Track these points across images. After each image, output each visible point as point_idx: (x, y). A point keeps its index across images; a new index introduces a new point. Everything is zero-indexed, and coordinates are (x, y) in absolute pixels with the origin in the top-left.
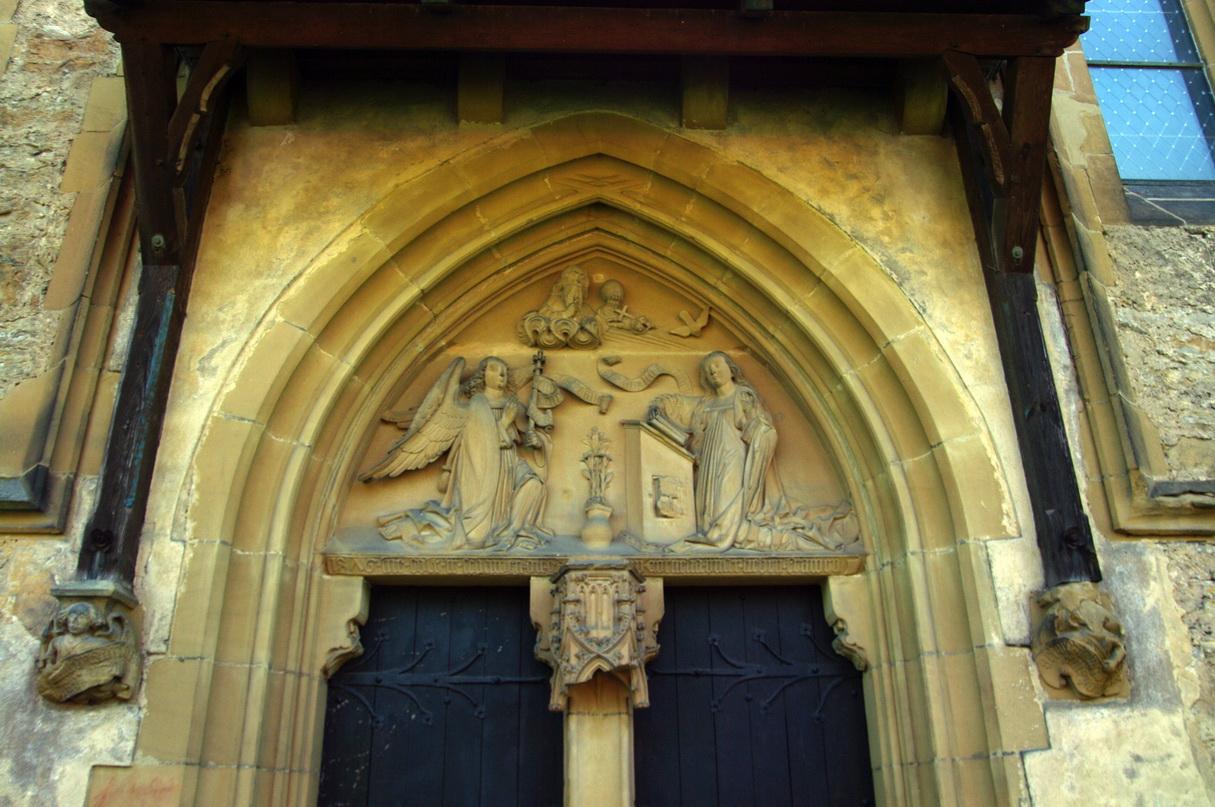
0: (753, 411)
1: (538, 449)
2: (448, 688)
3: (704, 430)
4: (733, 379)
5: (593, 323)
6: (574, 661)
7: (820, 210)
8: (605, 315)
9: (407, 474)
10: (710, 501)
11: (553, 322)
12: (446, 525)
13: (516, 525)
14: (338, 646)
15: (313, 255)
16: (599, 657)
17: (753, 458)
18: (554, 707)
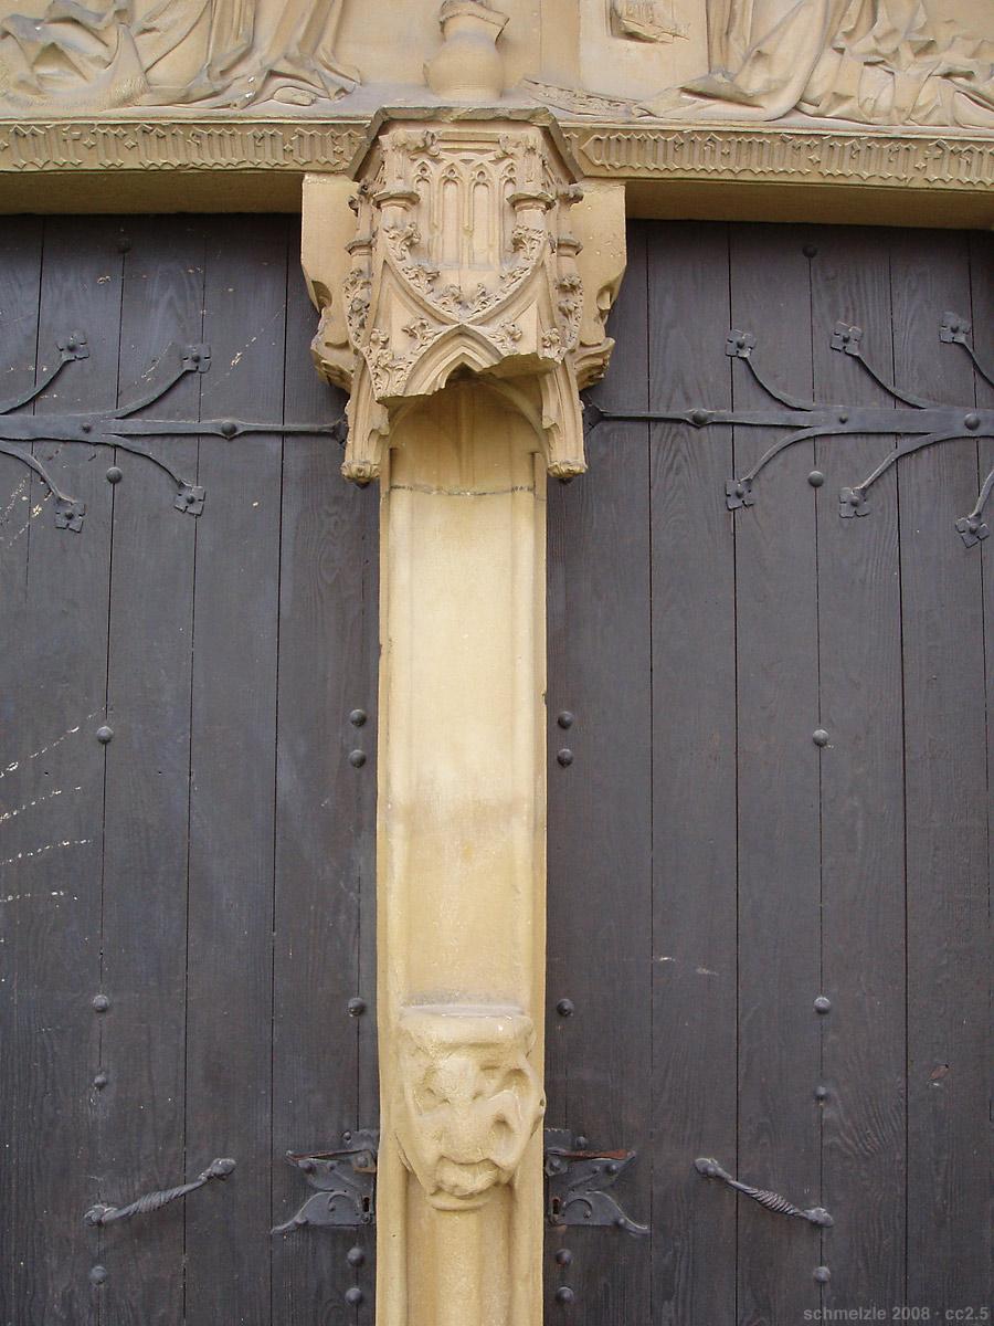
2: (116, 447)
6: (399, 342)
12: (97, 49)
13: (267, 51)
16: (462, 332)
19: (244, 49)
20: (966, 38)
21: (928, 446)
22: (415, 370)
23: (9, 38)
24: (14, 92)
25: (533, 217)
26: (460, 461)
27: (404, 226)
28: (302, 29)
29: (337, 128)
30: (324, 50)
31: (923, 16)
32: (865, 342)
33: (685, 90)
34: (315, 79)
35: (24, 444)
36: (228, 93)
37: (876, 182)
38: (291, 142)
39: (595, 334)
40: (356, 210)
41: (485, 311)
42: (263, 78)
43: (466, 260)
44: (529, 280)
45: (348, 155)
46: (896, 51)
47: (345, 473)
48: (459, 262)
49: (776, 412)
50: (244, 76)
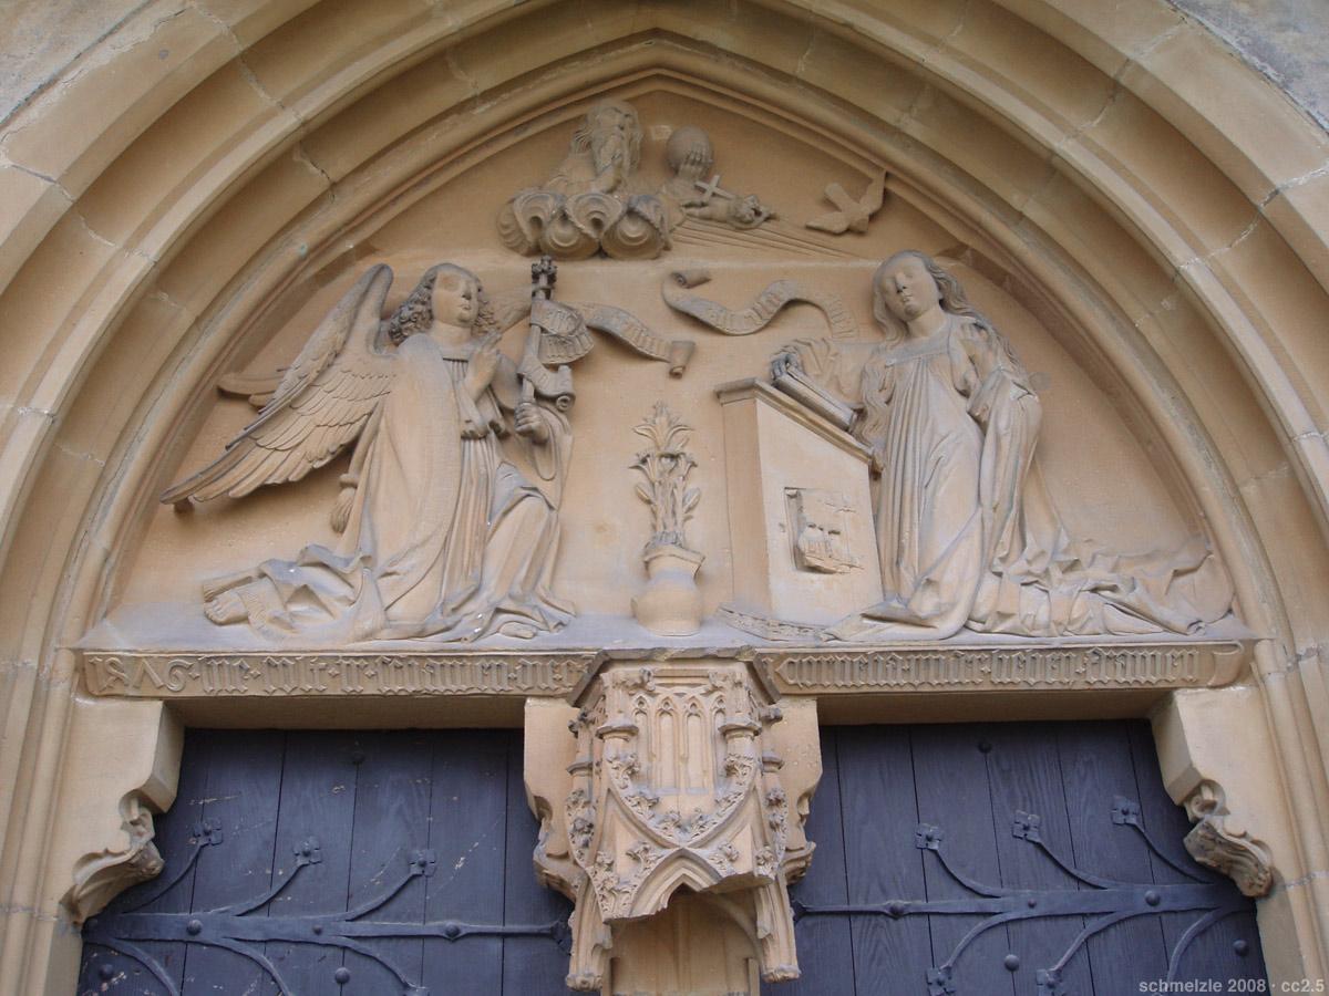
0: (990, 356)
1: (538, 441)
2: (345, 948)
3: (888, 402)
4: (942, 303)
5: (653, 203)
6: (623, 865)
9: (267, 493)
10: (912, 536)
11: (571, 201)
12: (344, 590)
13: (492, 592)
14: (100, 850)
17: (998, 446)
18: (579, 980)
19: (473, 589)
20: (1106, 555)
21: (1114, 924)
22: (640, 893)
23: (266, 578)
25: (744, 746)
26: (677, 965)
27: (626, 757)
29: (559, 659)
30: (544, 588)
31: (1066, 538)
32: (1044, 828)
33: (866, 616)
35: (257, 945)
36: (459, 628)
37: (1042, 687)
38: (515, 671)
39: (793, 837)
40: (576, 734)
41: (703, 835)
44: (742, 804)
45: (569, 683)
46: (1047, 571)
47: (570, 984)
48: (676, 786)
49: (967, 899)
50: (472, 613)
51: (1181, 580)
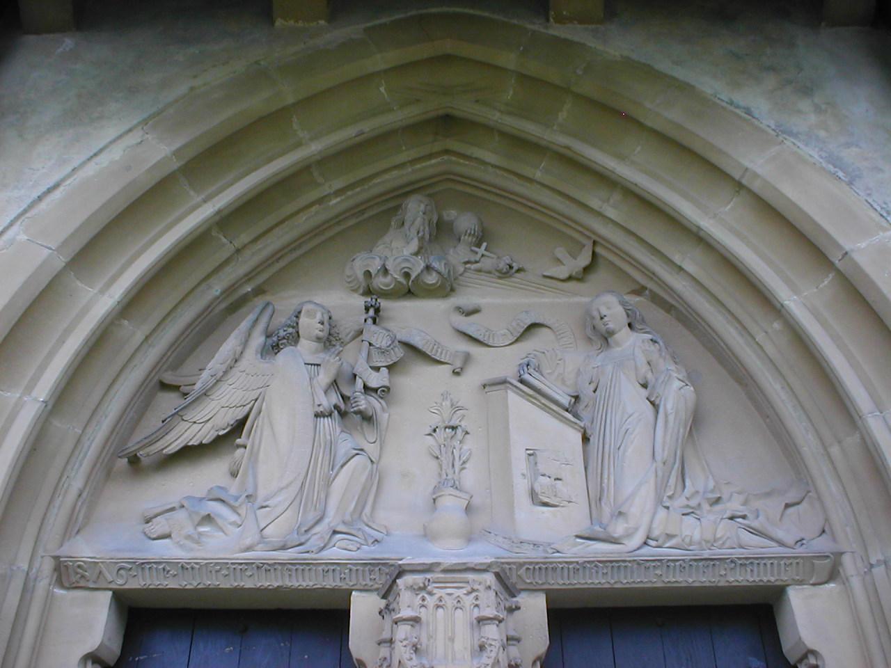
4: (630, 325)
7: (731, 103)
8: (458, 254)
12: (233, 517)
13: (331, 520)
15: (76, 164)
17: (666, 422)
19: (319, 517)
20: (739, 493)
23: (183, 509)
24: (183, 542)
25: (492, 632)
28: (354, 503)
29: (375, 565)
30: (366, 515)
34: (360, 534)
36: (308, 544)
37: (696, 584)
38: (345, 574)
40: (383, 617)
42: (329, 535)
43: (450, 658)
45: (381, 581)
46: (699, 505)
51: (791, 510)
